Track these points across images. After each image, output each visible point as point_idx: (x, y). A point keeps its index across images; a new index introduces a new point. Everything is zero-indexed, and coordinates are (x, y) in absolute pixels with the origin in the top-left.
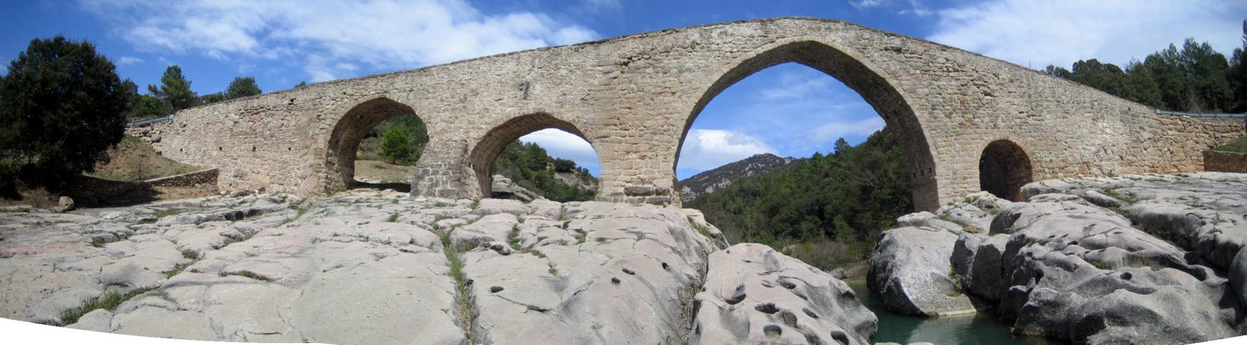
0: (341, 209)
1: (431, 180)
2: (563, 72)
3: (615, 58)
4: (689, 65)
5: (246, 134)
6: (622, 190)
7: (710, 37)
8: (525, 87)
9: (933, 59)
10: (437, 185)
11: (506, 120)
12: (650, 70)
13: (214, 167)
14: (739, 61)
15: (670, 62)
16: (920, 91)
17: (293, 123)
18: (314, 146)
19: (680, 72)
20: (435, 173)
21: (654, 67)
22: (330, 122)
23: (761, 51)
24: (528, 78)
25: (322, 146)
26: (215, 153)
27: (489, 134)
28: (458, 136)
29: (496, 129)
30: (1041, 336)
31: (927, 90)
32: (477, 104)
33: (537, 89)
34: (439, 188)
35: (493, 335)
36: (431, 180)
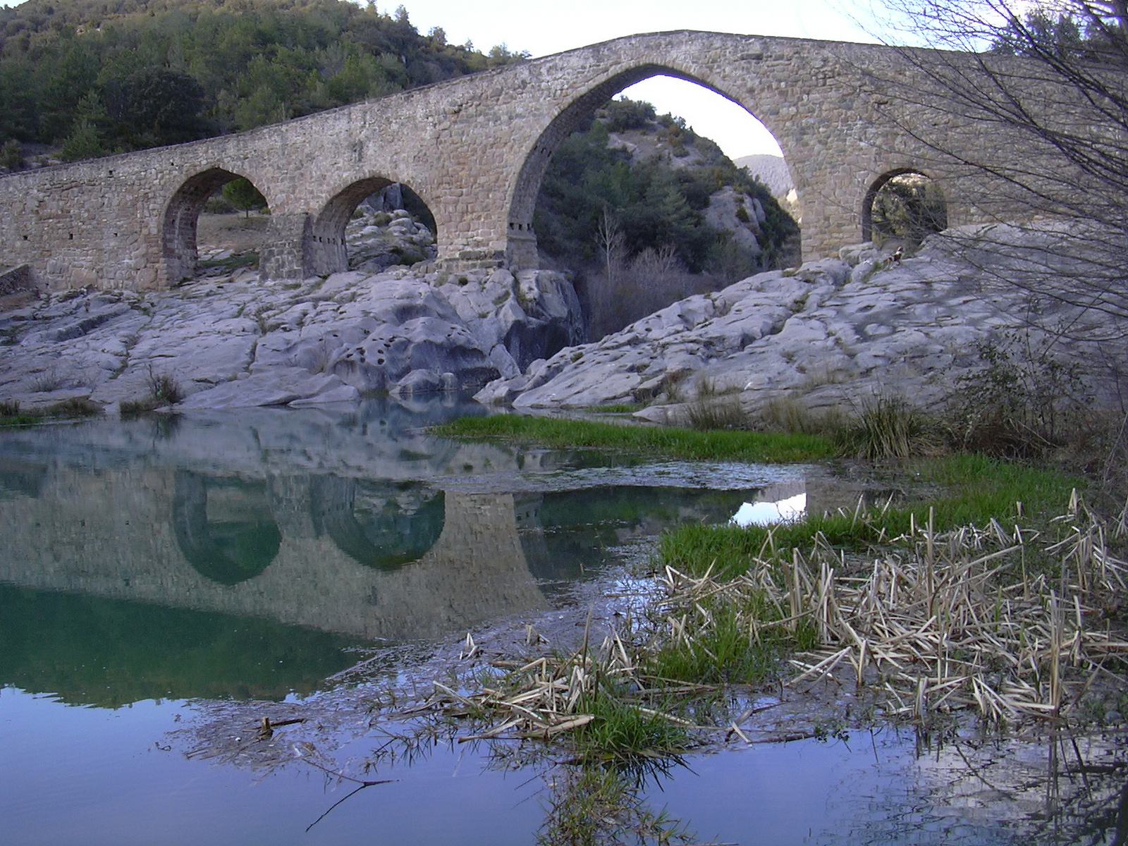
0: (193, 307)
1: (277, 260)
2: (394, 127)
3: (444, 105)
4: (519, 110)
5: (57, 217)
6: (457, 256)
7: (540, 74)
8: (358, 148)
9: (804, 63)
10: (283, 266)
11: (343, 186)
12: (481, 119)
13: (20, 264)
14: (569, 100)
15: (501, 109)
16: (784, 111)
17: (115, 202)
18: (145, 231)
19: (511, 118)
20: (281, 253)
21: (486, 115)
22: (159, 204)
23: (592, 84)
24: (362, 136)
25: (154, 231)
26: (18, 244)
27: (330, 202)
28: (300, 208)
29: (336, 197)
30: (500, 328)
31: (793, 110)
32: (314, 170)
33: (371, 149)
34: (286, 269)
35: (27, 188)
36: (277, 260)
